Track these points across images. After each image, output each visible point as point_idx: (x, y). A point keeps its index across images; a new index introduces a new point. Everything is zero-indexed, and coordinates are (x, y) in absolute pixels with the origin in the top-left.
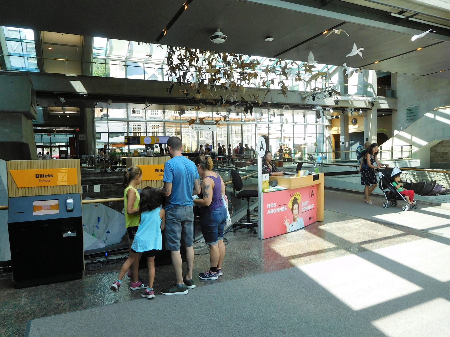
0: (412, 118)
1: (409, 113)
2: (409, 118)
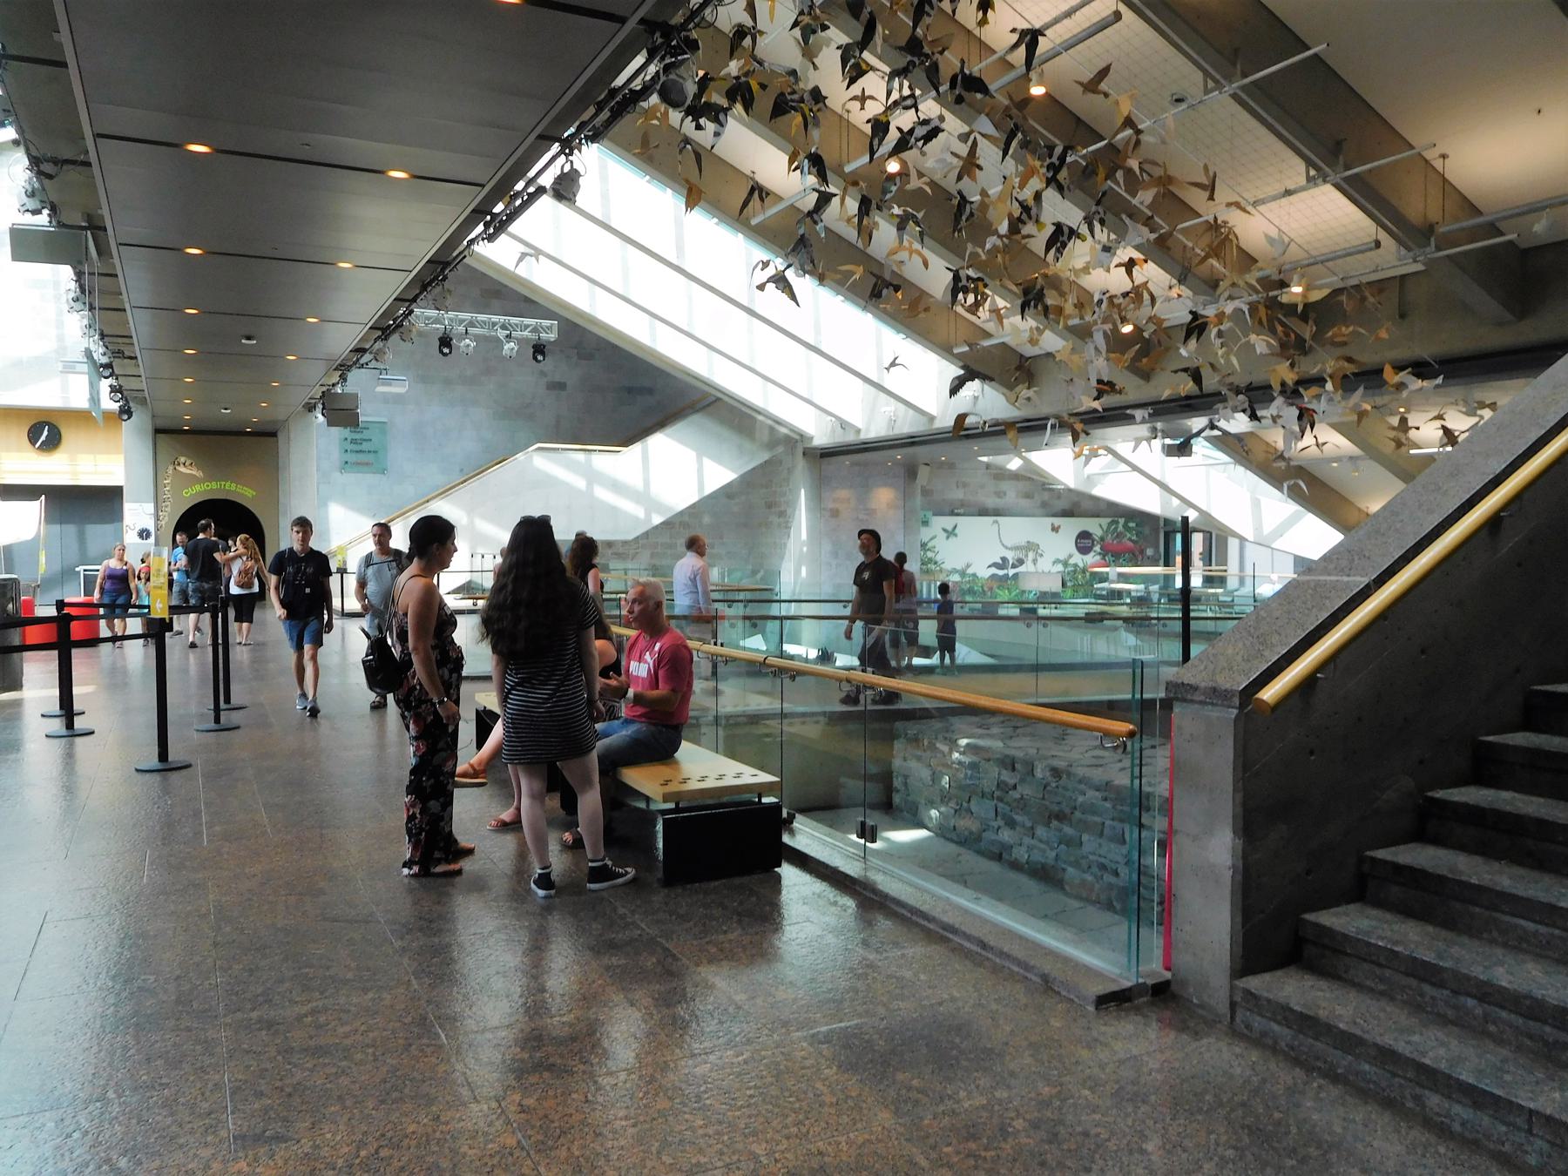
0: (362, 458)
1: (354, 441)
2: (352, 458)
